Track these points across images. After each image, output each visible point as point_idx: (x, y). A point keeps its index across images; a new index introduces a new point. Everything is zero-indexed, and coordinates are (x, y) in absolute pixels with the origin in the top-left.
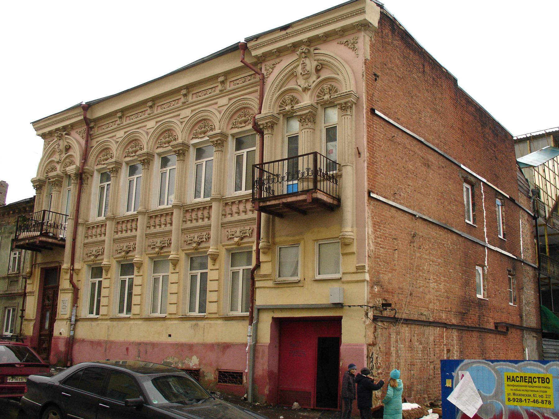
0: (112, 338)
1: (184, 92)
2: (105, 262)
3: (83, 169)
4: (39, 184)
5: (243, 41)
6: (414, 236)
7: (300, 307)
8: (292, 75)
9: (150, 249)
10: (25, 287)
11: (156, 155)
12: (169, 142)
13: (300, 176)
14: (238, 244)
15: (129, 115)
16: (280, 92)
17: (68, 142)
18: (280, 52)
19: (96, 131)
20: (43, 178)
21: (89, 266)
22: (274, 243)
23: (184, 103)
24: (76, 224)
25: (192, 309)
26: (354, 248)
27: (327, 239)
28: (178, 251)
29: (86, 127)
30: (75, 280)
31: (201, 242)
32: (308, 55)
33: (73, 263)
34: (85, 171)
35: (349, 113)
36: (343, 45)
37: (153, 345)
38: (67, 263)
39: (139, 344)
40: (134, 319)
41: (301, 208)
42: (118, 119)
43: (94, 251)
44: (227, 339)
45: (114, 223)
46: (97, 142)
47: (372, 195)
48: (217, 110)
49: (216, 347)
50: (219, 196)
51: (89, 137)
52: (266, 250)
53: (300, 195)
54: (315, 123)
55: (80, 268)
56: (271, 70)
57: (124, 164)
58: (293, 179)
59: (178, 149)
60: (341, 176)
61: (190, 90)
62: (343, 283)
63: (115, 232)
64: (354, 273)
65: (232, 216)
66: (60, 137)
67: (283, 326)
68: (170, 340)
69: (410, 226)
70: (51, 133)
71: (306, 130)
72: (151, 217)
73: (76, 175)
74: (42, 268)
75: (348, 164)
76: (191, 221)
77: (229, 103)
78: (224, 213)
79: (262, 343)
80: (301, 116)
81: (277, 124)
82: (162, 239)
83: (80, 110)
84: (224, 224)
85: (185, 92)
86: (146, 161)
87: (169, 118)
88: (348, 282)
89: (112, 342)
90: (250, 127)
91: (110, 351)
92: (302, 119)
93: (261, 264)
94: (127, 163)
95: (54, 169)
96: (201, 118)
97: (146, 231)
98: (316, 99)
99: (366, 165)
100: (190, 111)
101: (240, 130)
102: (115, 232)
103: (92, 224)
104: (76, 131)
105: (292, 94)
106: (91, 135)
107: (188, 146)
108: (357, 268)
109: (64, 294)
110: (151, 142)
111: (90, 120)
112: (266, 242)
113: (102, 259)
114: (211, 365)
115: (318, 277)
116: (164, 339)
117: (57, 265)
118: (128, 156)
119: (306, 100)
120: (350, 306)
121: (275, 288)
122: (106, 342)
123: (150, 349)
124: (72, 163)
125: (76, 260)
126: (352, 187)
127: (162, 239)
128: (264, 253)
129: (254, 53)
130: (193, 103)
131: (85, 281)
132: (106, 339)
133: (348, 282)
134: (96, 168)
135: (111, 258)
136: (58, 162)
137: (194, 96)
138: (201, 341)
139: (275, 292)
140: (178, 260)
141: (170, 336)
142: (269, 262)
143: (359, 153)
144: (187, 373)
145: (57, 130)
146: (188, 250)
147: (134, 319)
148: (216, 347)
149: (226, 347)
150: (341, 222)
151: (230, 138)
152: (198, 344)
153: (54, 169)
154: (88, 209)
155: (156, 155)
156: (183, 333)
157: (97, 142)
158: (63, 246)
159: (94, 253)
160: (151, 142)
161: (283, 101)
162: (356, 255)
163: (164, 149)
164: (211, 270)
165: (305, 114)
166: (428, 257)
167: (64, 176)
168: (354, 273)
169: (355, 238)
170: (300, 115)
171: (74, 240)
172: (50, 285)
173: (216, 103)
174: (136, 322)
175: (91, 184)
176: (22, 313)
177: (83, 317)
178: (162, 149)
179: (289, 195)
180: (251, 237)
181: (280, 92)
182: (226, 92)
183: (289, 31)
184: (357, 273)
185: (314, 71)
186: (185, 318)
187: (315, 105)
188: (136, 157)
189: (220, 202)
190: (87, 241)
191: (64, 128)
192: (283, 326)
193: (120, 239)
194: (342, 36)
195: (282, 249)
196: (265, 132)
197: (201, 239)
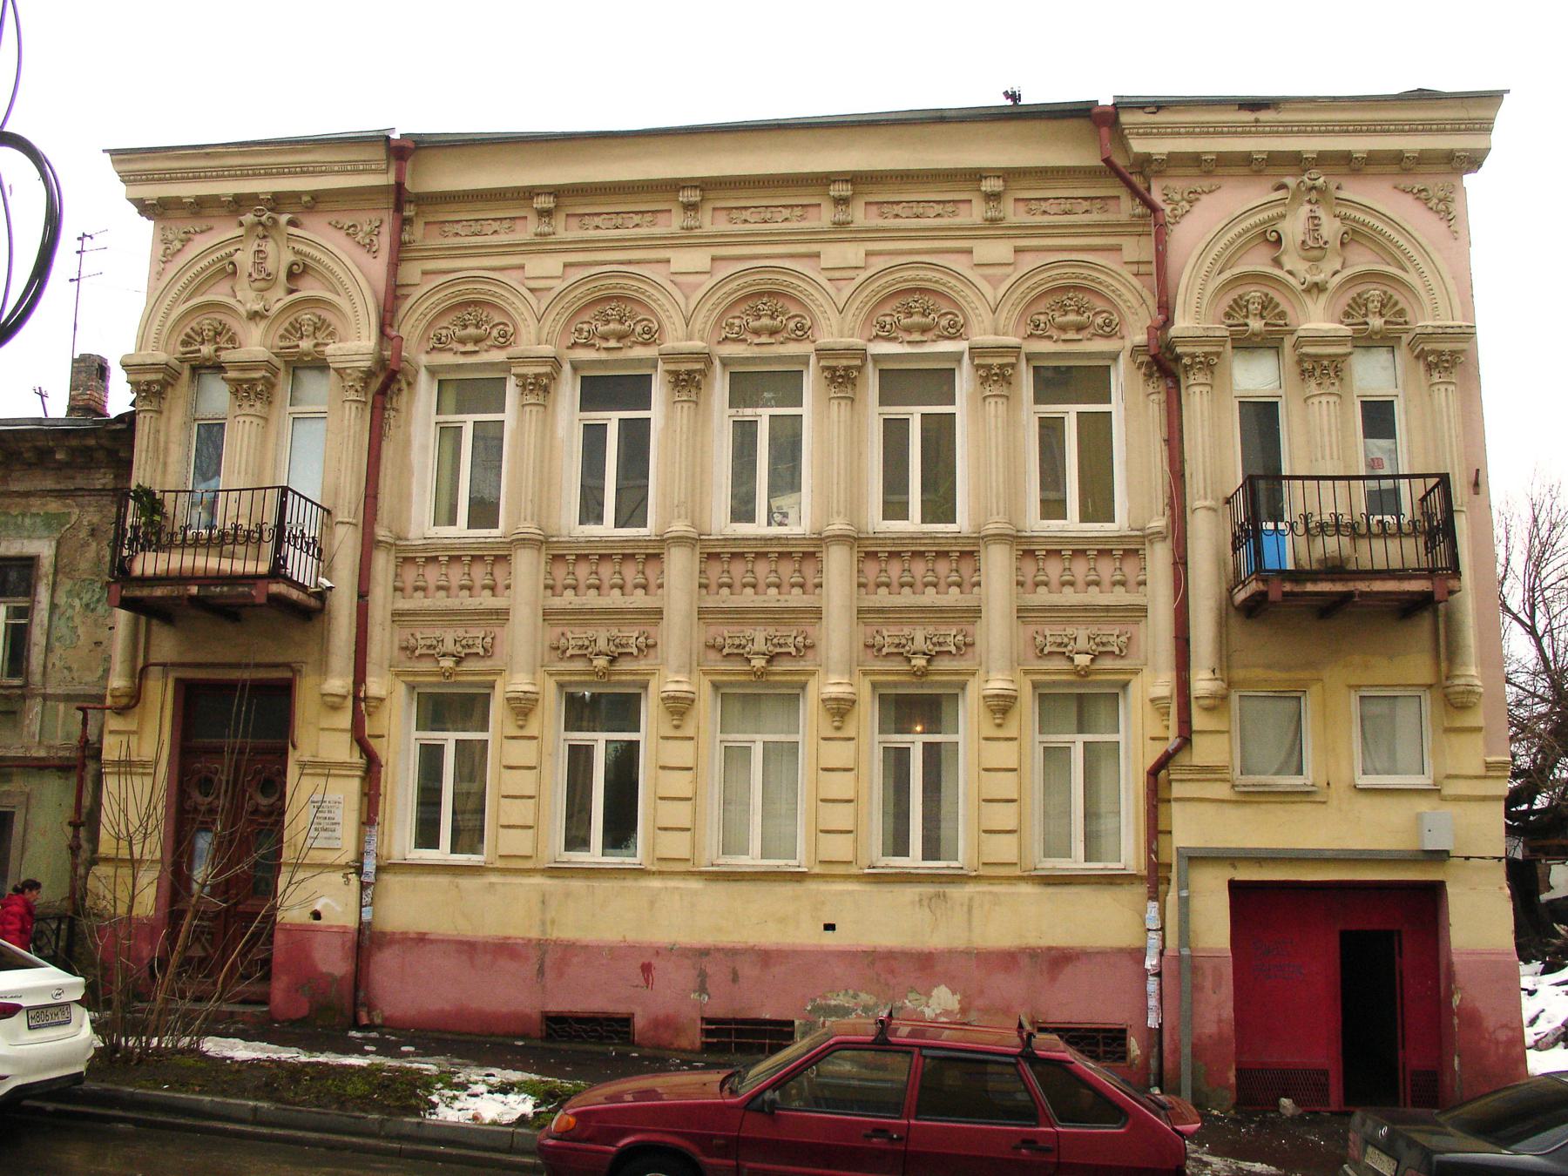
0: (555, 934)
1: (692, 196)
5: (1106, 100)
7: (1328, 855)
8: (229, 271)
9: (713, 655)
16: (1227, 275)
17: (298, 253)
18: (1248, 166)
21: (412, 687)
24: (369, 544)
25: (899, 846)
32: (273, 232)
36: (343, 233)
37: (766, 957)
38: (341, 675)
39: (704, 952)
40: (661, 873)
44: (1059, 937)
49: (1025, 961)
56: (178, 245)
59: (845, 363)
62: (1444, 799)
64: (1476, 777)
66: (266, 230)
67: (1248, 901)
68: (829, 940)
70: (200, 206)
71: (248, 420)
74: (178, 681)
78: (398, 584)
79: (1204, 949)
83: (380, 153)
84: (1027, 610)
88: (1458, 799)
89: (569, 949)
91: (561, 974)
93: (1195, 738)
101: (603, 356)
104: (333, 218)
114: (1007, 1011)
115: (1365, 781)
116: (807, 935)
117: (289, 674)
118: (585, 345)
119: (255, 344)
120: (1467, 858)
122: (542, 945)
123: (748, 970)
128: (1209, 710)
129: (1138, 146)
131: (401, 739)
132: (534, 934)
133: (1458, 799)
134: (424, 359)
135: (539, 670)
136: (254, 316)
138: (960, 943)
139: (1233, 813)
140: (854, 702)
141: (830, 927)
144: (1069, 1042)
145: (239, 203)
146: (723, 673)
147: (661, 873)
148: (1025, 961)
149: (1059, 960)
152: (951, 953)
154: (404, 497)
156: (888, 921)
157: (425, 273)
163: (756, 349)
165: (1330, 356)
168: (1476, 777)
170: (1316, 356)
171: (363, 595)
176: (76, 836)
183: (1264, 116)
184: (1485, 777)
185: (283, 275)
191: (277, 201)
194: (1406, 171)
195: (1295, 703)
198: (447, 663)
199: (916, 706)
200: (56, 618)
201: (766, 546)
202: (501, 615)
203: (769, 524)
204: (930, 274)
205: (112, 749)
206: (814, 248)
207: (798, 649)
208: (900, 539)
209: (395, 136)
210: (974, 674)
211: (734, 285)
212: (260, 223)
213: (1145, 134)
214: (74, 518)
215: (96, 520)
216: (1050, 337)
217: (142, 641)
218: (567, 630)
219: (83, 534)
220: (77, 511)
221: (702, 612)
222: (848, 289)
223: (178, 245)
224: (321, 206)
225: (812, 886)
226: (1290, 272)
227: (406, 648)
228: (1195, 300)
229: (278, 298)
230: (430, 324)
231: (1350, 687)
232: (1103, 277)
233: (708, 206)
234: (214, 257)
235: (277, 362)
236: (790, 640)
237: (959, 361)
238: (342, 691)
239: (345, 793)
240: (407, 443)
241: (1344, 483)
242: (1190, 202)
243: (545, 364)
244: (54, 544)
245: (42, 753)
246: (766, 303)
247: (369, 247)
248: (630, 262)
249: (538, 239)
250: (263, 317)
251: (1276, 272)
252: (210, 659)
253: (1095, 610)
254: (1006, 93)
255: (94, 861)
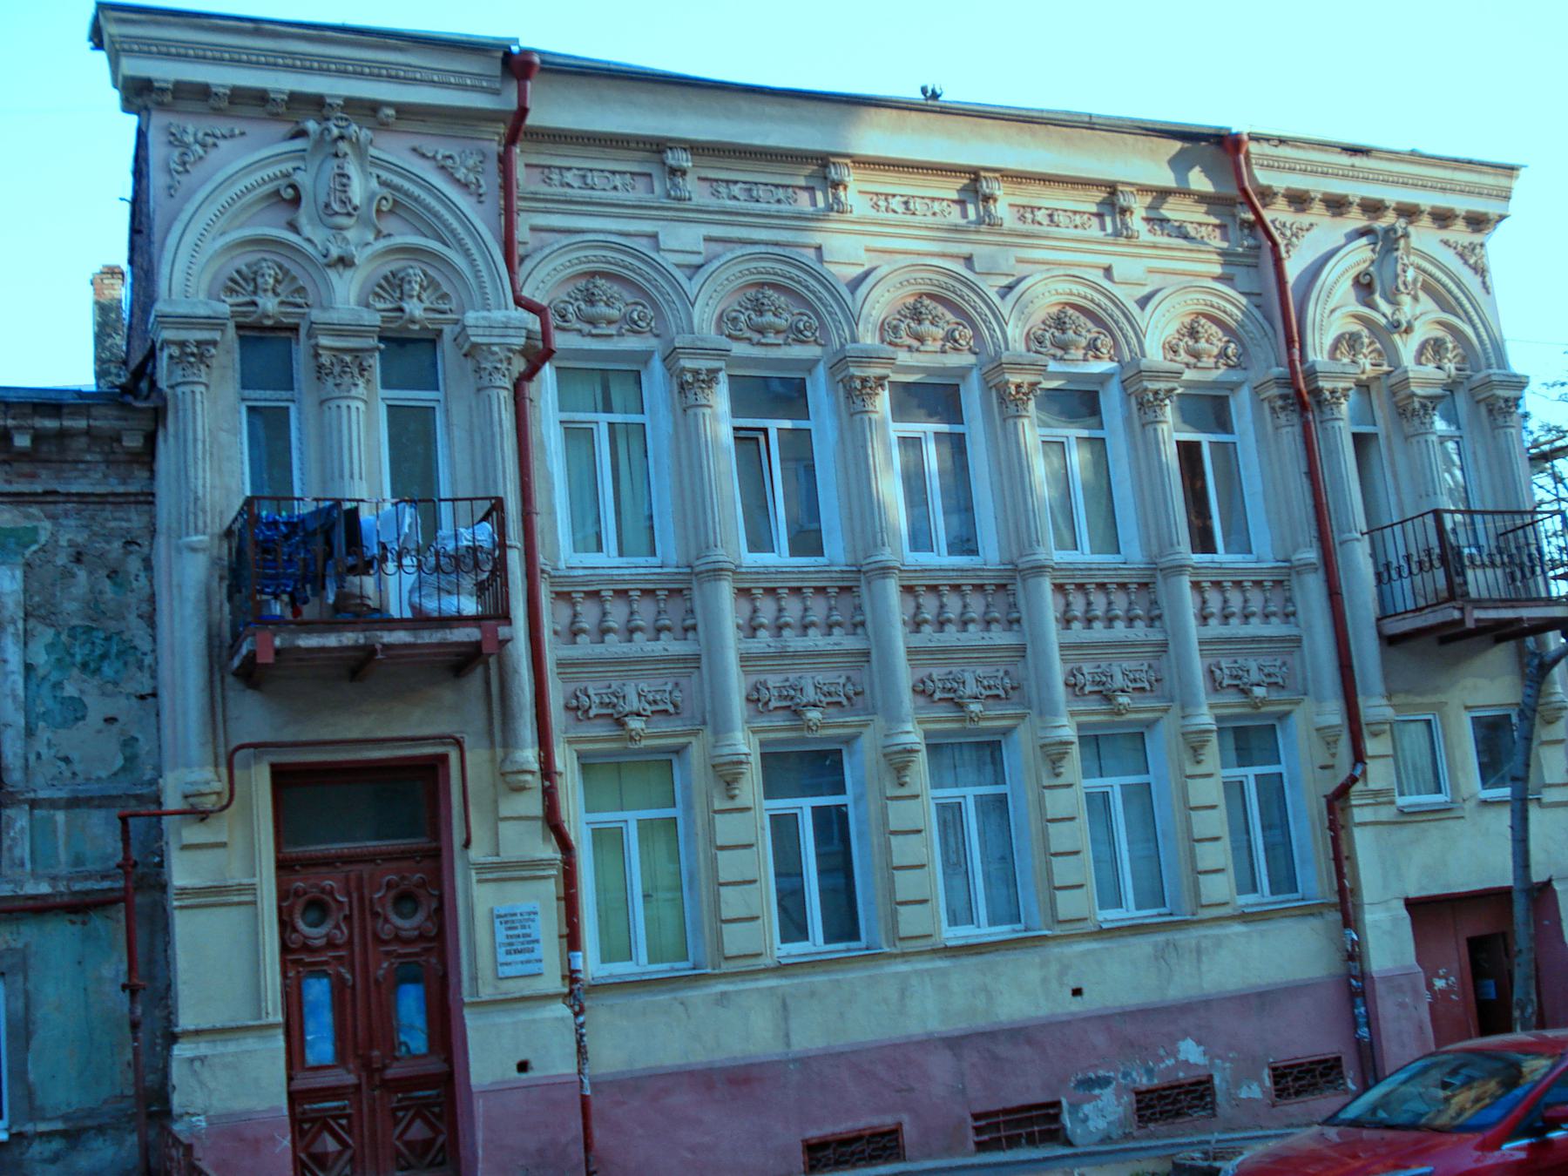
68: (1076, 1006)
84: (918, 653)
104: (416, 141)
141: (1077, 992)
199: (809, 766)
200: (33, 687)
205: (182, 872)
208: (765, 571)
209: (515, 49)
213: (178, 55)
214: (43, 537)
215: (81, 538)
217: (220, 718)
219: (62, 559)
220: (47, 524)
225: (1055, 950)
226: (309, 240)
237: (646, 363)
242: (204, 146)
244: (19, 574)
245: (45, 888)
251: (291, 237)
254: (924, 90)
255: (173, 1038)
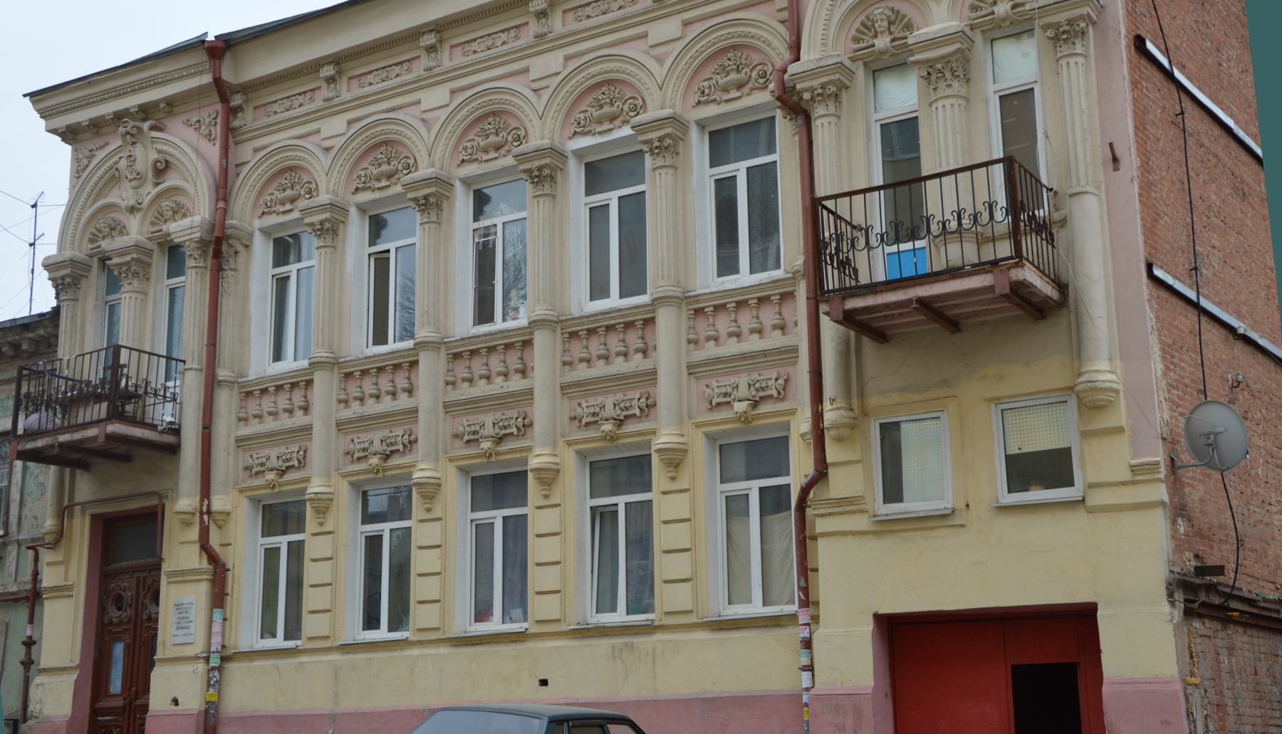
1: (429, 39)
2: (316, 486)
3: (223, 226)
4: (67, 276)
6: (1237, 384)
9: (458, 443)
10: (36, 574)
11: (458, 184)
12: (293, 201)
13: (935, 229)
14: (744, 419)
15: (357, 72)
16: (95, 207)
17: (160, 152)
19: (246, 120)
20: (80, 255)
21: (255, 501)
22: (865, 413)
23: (539, 36)
24: (211, 384)
26: (1120, 416)
27: (1013, 396)
28: (555, 446)
29: (219, 107)
30: (214, 541)
31: (392, 452)
33: (206, 492)
34: (228, 232)
35: (1079, 49)
41: (875, 325)
42: (324, 85)
43: (274, 458)
45: (336, 376)
46: (256, 150)
47: (1158, 272)
48: (319, 146)
50: (677, 292)
51: (230, 136)
52: (845, 432)
53: (969, 274)
54: (968, 80)
55: (229, 508)
57: (353, 212)
58: (913, 236)
59: (537, 163)
60: (1063, 222)
61: (446, 35)
63: (340, 401)
64: (1124, 483)
65: (783, 334)
66: (133, 137)
67: (902, 635)
69: (1225, 357)
70: (97, 126)
71: (948, 102)
72: (457, 356)
73: (203, 244)
74: (95, 518)
75: (1088, 189)
76: (362, 400)
77: (451, 100)
80: (930, 63)
81: (847, 88)
82: (498, 415)
83: (201, 57)
85: (434, 41)
86: (432, 200)
87: (388, 111)
90: (764, 97)
92: (934, 73)
93: (831, 471)
94: (362, 209)
95: (117, 229)
96: (599, 79)
97: (445, 393)
98: (967, 13)
99: (1136, 190)
100: (561, 60)
101: (377, 195)
102: (340, 401)
103: (258, 381)
104: (185, 117)
105: (112, 215)
106: (234, 130)
107: (344, 211)
108: (1134, 469)
109: (182, 587)
110: (440, 148)
111: (230, 86)
112: (846, 409)
113: (307, 480)
117: (155, 502)
118: (365, 189)
121: (875, 533)
124: (180, 211)
125: (216, 485)
126: (1102, 248)
127: (498, 415)
128: (839, 440)
130: (570, 35)
131: (246, 546)
134: (257, 223)
136: (132, 210)
137: (571, 16)
140: (558, 471)
141: (544, 683)
142: (857, 462)
143: (1115, 160)
145: (119, 116)
150: (1077, 349)
151: (694, 132)
153: (117, 229)
154: (244, 341)
155: (458, 184)
157: (256, 150)
158: (173, 450)
159: (273, 463)
160: (440, 148)
161: (863, 24)
162: (1125, 438)
164: (665, 493)
165: (942, 57)
166: (1262, 444)
167: (155, 247)
168: (1124, 483)
169: (1120, 387)
170: (928, 61)
172: (124, 564)
173: (644, 36)
174: (426, 651)
175: (247, 270)
177: (244, 646)
178: (274, 216)
179: (890, 285)
180: (783, 400)
181: (95, 207)
182: (554, 40)
184: (1133, 483)
185: (150, 174)
186: (585, 632)
187: (848, 63)
188: (296, 214)
189: (680, 307)
190: (245, 431)
191: (145, 111)
192: (902, 635)
193: (361, 419)
196: (818, 110)
197: (288, 460)
198: (271, 476)
199: (500, 486)
201: (493, 340)
202: (307, 429)
203: (504, 320)
204: (612, 65)
205: (49, 578)
206: (524, 63)
207: (518, 429)
210: (794, 414)
211: (464, 112)
212: (128, 133)
216: (714, 101)
218: (354, 436)
221: (448, 407)
222: (546, 95)
223: (85, 162)
224: (176, 109)
225: (530, 645)
227: (348, 453)
228: (820, 32)
229: (149, 191)
230: (260, 193)
231: (989, 400)
232: (753, 31)
233: (447, 46)
234: (105, 167)
235: (150, 245)
236: (512, 422)
238: (190, 509)
239: (198, 594)
240: (246, 298)
241: (906, 188)
243: (325, 211)
246: (491, 123)
247: (209, 137)
248: (393, 110)
249: (326, 104)
250: (139, 210)
252: (112, 495)
253: (753, 357)
